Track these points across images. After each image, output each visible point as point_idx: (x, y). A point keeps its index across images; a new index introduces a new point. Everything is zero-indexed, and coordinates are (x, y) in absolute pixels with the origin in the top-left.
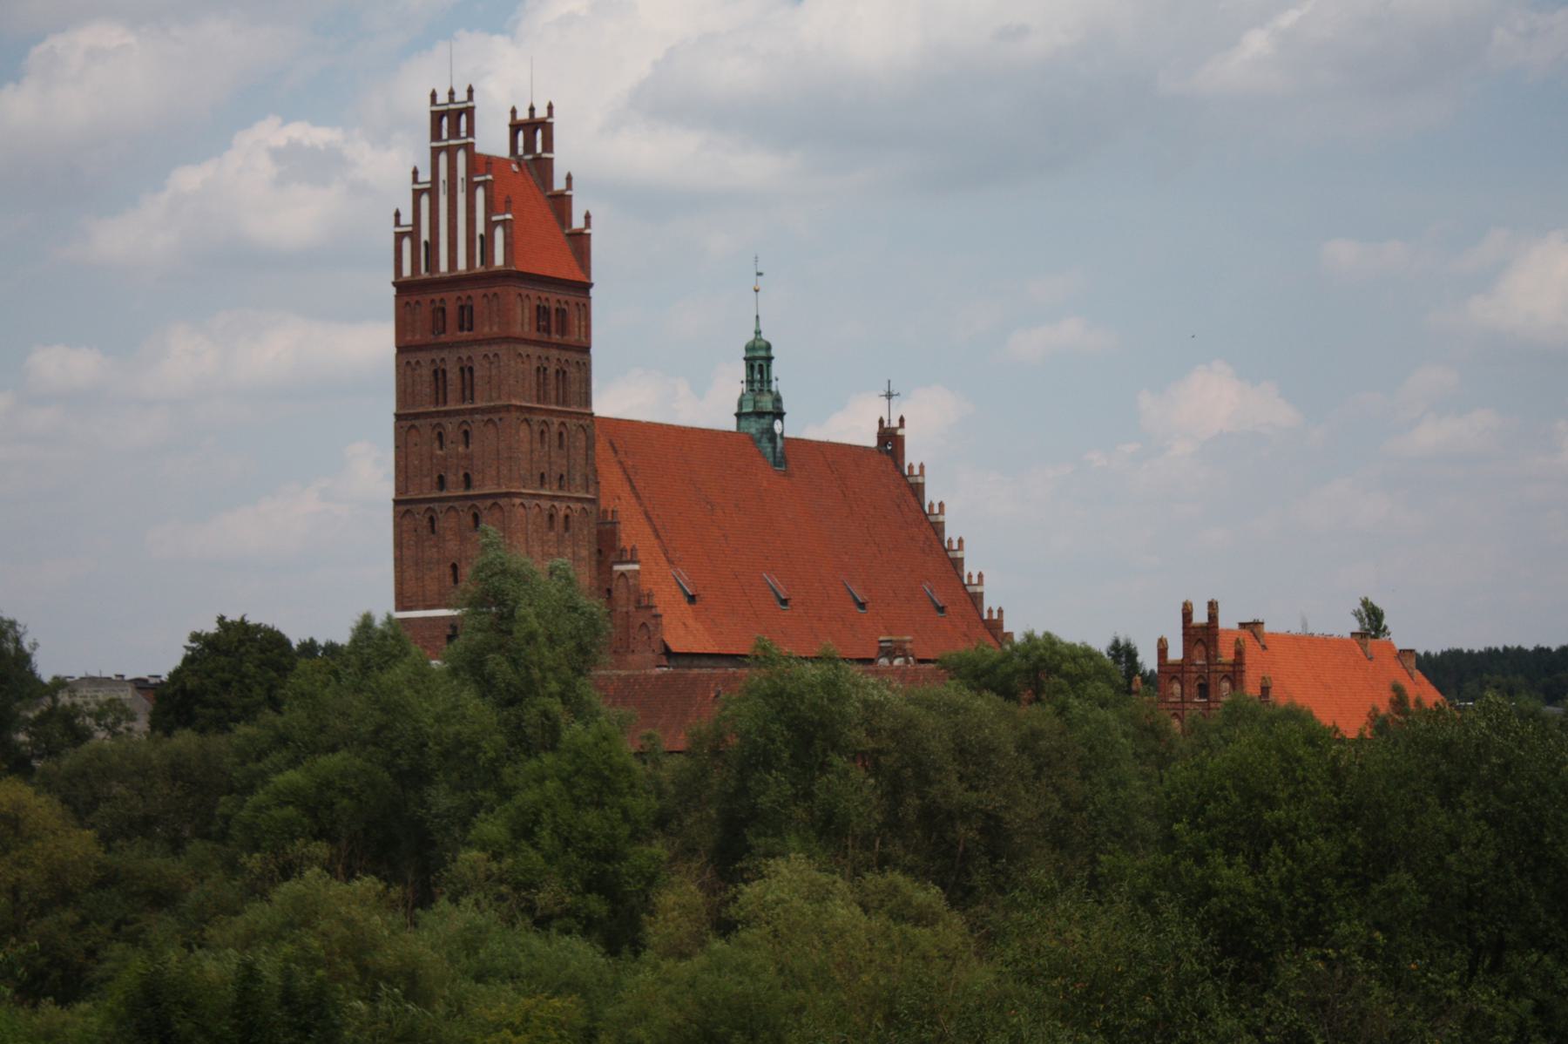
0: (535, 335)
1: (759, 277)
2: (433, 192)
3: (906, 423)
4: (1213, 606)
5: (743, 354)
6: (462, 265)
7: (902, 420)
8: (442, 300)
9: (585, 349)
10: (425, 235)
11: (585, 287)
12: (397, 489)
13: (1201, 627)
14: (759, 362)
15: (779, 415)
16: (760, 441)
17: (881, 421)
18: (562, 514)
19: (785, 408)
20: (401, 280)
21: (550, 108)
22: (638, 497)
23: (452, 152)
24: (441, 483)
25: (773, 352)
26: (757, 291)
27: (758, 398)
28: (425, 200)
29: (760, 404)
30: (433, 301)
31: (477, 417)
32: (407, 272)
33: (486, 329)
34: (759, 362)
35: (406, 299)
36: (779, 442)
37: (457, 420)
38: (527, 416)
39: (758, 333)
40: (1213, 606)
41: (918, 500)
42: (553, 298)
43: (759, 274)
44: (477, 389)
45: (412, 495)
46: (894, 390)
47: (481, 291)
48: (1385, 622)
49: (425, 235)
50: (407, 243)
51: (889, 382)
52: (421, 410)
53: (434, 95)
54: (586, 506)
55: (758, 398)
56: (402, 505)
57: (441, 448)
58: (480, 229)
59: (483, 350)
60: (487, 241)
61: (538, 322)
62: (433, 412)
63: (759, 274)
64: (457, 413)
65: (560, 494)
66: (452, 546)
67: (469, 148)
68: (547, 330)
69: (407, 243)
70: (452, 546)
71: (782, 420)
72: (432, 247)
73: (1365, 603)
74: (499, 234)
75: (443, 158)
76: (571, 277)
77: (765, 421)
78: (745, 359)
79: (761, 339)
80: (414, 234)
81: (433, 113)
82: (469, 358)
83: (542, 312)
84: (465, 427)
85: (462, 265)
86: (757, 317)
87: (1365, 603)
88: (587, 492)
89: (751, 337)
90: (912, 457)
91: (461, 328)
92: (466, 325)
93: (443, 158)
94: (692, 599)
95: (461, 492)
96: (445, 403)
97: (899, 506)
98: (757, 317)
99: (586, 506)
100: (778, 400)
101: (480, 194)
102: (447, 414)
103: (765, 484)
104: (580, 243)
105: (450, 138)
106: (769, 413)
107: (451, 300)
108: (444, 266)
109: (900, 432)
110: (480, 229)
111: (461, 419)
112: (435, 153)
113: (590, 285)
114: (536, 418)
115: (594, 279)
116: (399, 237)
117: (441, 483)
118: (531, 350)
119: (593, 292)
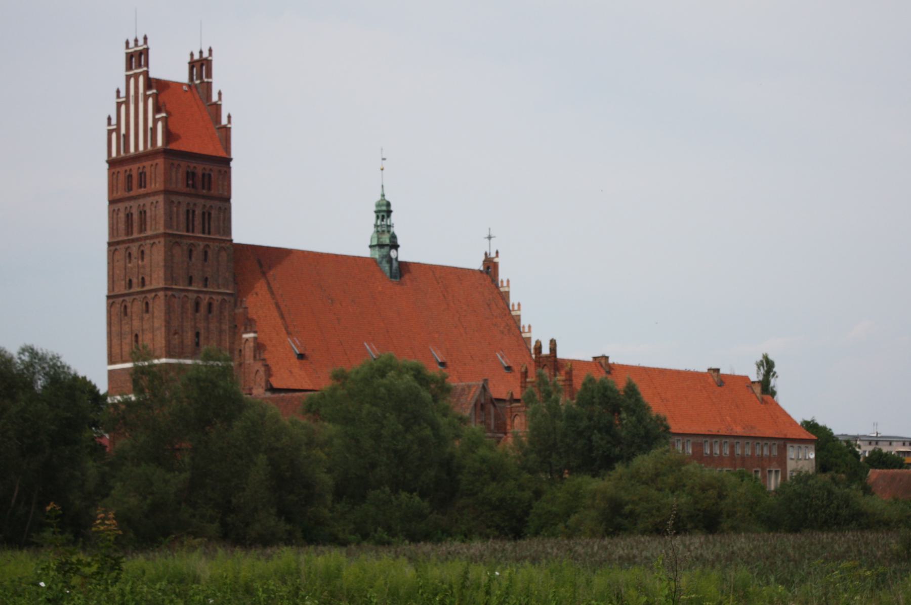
0: (188, 190)
1: (384, 161)
2: (127, 103)
3: (500, 254)
4: (553, 344)
5: (374, 209)
6: (141, 148)
7: (497, 252)
8: (131, 170)
9: (227, 199)
10: (123, 131)
11: (228, 160)
12: (109, 289)
13: (547, 357)
14: (384, 211)
15: (395, 246)
16: (381, 263)
17: (486, 254)
18: (206, 302)
19: (399, 242)
20: (111, 159)
21: (210, 50)
22: (272, 293)
23: (136, 76)
24: (130, 284)
25: (392, 208)
26: (382, 170)
27: (380, 236)
28: (123, 108)
29: (381, 240)
30: (126, 171)
31: (148, 241)
32: (114, 154)
33: (153, 186)
34: (384, 211)
35: (113, 170)
36: (395, 264)
37: (137, 244)
38: (178, 240)
39: (383, 195)
40: (553, 344)
41: (506, 302)
42: (199, 168)
43: (384, 159)
44: (148, 224)
45: (116, 292)
46: (493, 234)
47: (150, 163)
48: (775, 370)
49: (123, 131)
50: (114, 135)
51: (490, 229)
52: (120, 239)
53: (127, 43)
54: (225, 297)
55: (380, 236)
56: (111, 298)
57: (130, 262)
58: (150, 124)
59: (151, 199)
60: (154, 130)
61: (187, 181)
62: (126, 240)
63: (384, 159)
64: (138, 240)
65: (205, 289)
66: (136, 323)
67: (146, 73)
68: (193, 186)
69: (114, 135)
70: (136, 323)
71: (397, 250)
72: (127, 136)
73: (766, 358)
74: (160, 126)
75: (132, 81)
76: (214, 154)
77: (386, 250)
78: (376, 212)
79: (384, 200)
80: (118, 130)
81: (127, 54)
82: (144, 205)
83: (190, 175)
84: (142, 248)
85: (141, 148)
86: (383, 186)
87: (766, 358)
88: (228, 289)
89: (379, 198)
90: (503, 275)
91: (140, 186)
92: (143, 185)
93: (132, 81)
94: (301, 356)
95: (139, 289)
96: (193, 232)
97: (489, 305)
98: (383, 186)
99: (225, 297)
100: (393, 237)
101: (150, 102)
102: (133, 241)
103: (380, 288)
104: (225, 133)
105: (136, 68)
106: (387, 245)
107: (135, 168)
108: (132, 150)
109: (496, 260)
110: (150, 124)
111: (139, 243)
112: (128, 78)
113: (230, 160)
114: (185, 241)
115: (234, 154)
116: (110, 132)
117: (130, 284)
118: (181, 199)
119: (232, 164)
